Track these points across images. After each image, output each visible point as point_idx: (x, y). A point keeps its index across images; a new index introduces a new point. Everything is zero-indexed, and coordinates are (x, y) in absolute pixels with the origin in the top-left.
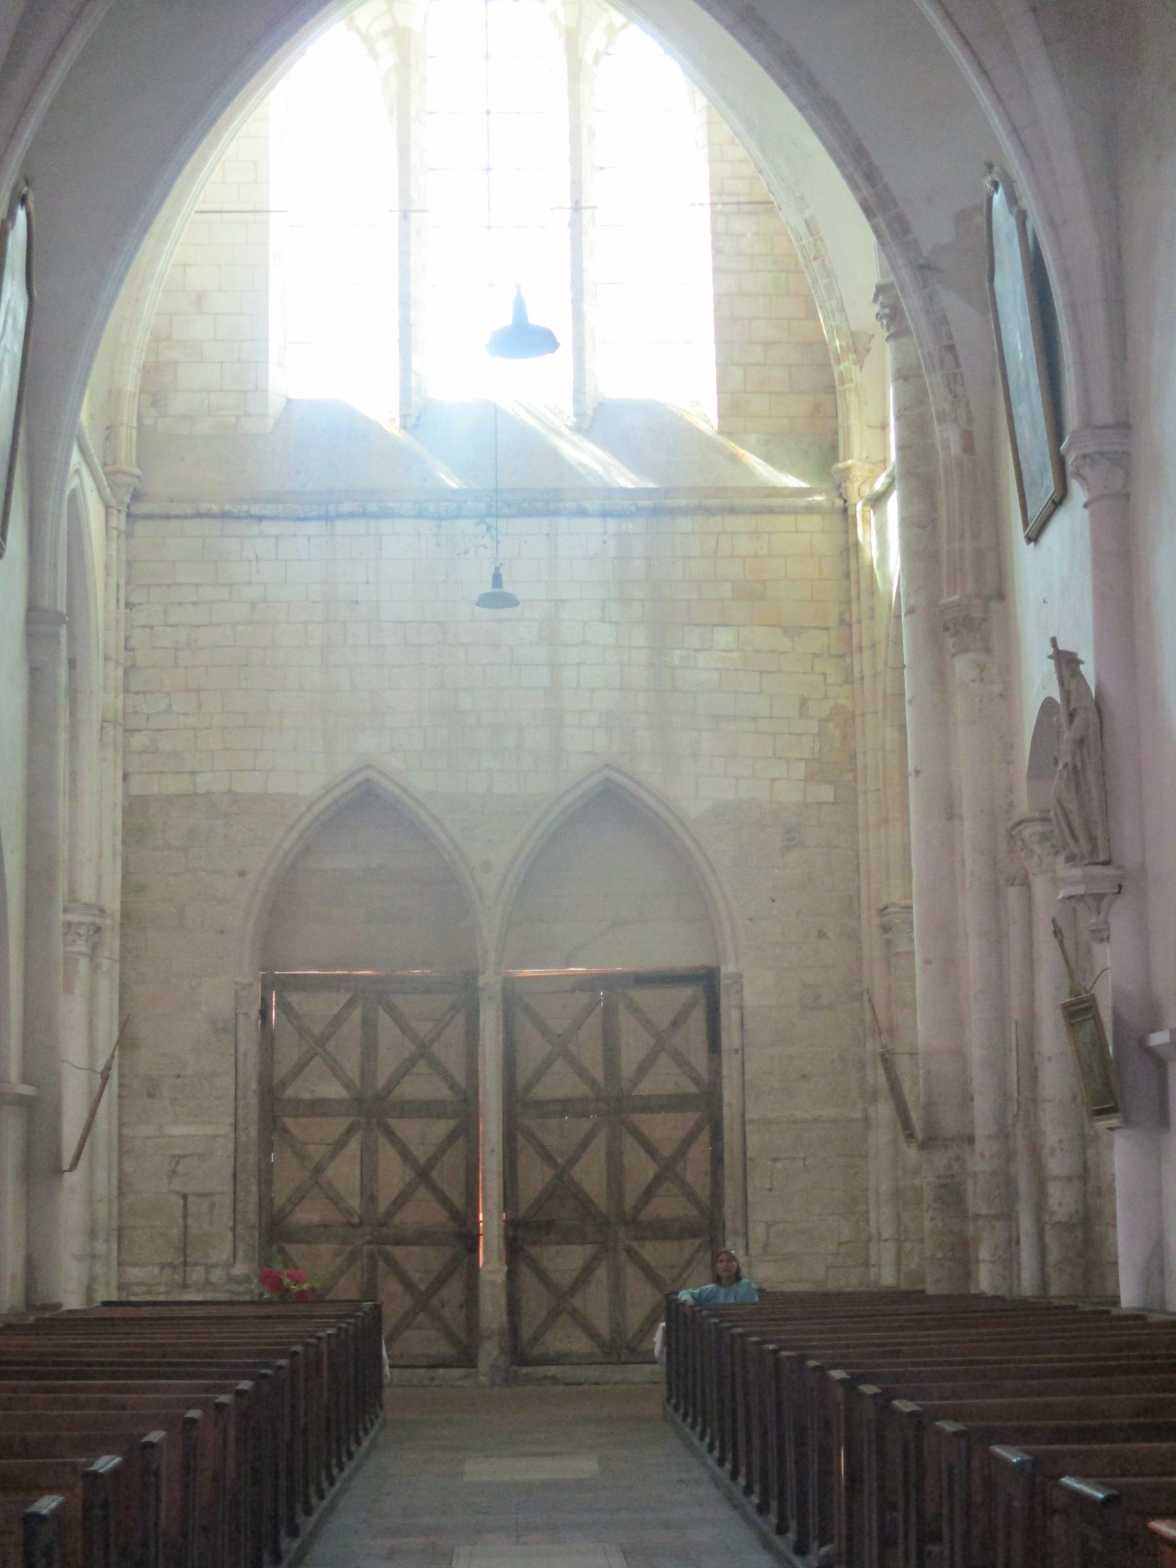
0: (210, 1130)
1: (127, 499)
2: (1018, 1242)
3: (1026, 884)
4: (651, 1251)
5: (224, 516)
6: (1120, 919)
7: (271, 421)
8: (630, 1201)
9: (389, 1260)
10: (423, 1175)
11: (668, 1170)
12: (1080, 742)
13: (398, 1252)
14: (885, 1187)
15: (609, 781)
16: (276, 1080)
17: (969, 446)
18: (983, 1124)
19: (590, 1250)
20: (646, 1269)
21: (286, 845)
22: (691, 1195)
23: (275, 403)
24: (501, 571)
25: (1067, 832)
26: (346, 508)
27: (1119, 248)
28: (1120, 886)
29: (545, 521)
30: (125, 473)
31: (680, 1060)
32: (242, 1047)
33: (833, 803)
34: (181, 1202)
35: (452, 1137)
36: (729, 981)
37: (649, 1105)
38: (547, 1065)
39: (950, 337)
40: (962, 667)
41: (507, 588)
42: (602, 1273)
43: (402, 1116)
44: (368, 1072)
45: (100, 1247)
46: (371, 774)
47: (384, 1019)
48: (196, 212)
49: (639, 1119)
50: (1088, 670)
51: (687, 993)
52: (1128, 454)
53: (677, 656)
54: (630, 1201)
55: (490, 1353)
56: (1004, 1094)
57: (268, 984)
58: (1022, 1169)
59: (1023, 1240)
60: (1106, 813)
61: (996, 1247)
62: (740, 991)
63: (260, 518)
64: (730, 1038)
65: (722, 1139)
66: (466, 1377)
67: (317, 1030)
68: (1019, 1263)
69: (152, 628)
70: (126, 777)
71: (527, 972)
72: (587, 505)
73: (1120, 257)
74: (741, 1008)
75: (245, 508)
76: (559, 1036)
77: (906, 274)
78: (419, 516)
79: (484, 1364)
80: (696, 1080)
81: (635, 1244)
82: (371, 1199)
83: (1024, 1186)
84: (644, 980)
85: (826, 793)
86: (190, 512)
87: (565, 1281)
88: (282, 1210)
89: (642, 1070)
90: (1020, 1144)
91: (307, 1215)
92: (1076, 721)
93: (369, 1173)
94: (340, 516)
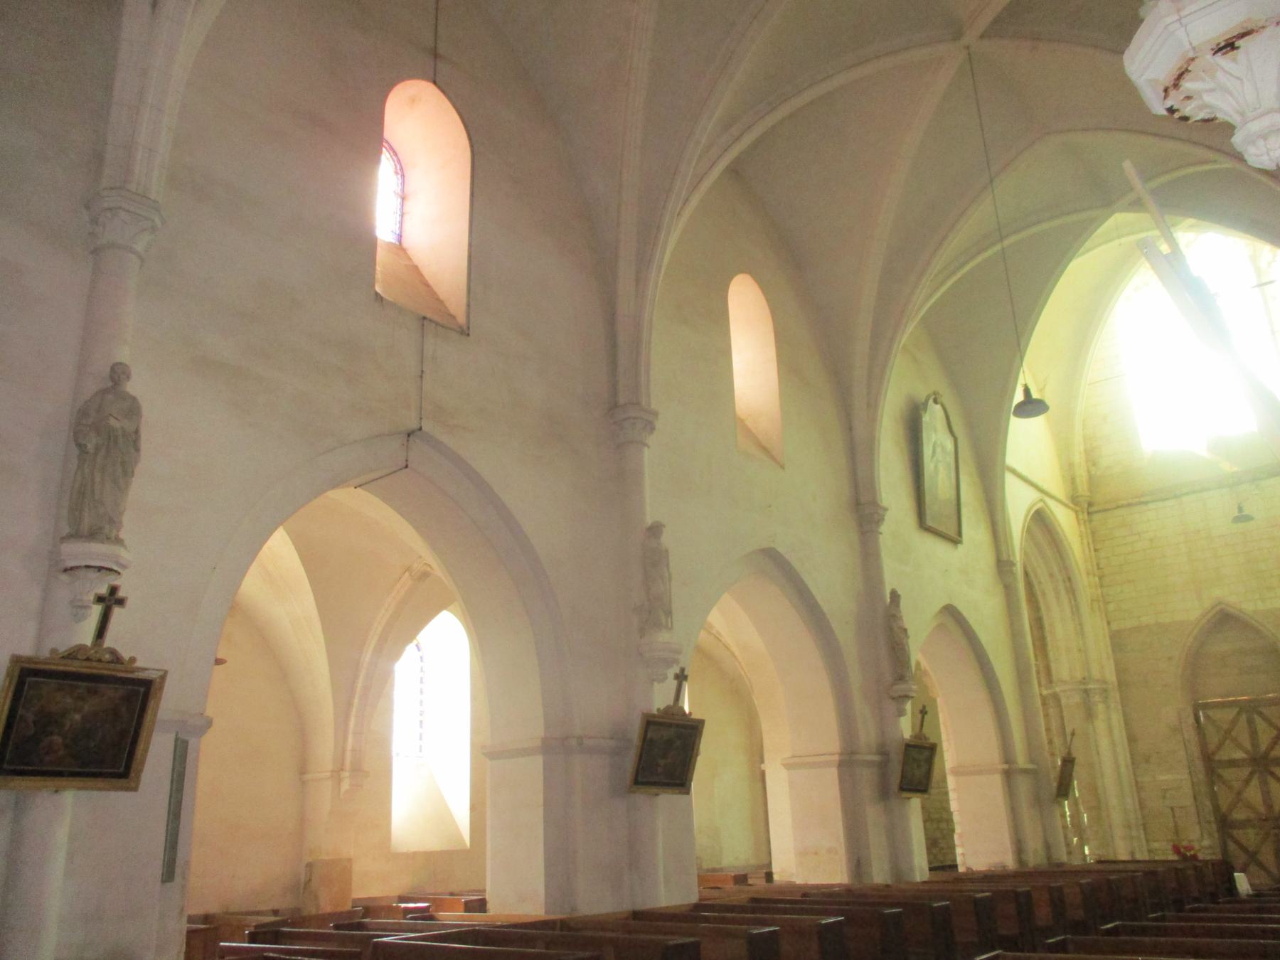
1: (1086, 506)
5: (1129, 505)
30: (1082, 496)
32: (1186, 736)
41: (1246, 512)
44: (1255, 744)
45: (1134, 833)
46: (1223, 606)
47: (1258, 720)
48: (1089, 384)
57: (1197, 708)
70: (1109, 623)
75: (1137, 500)
91: (1239, 815)
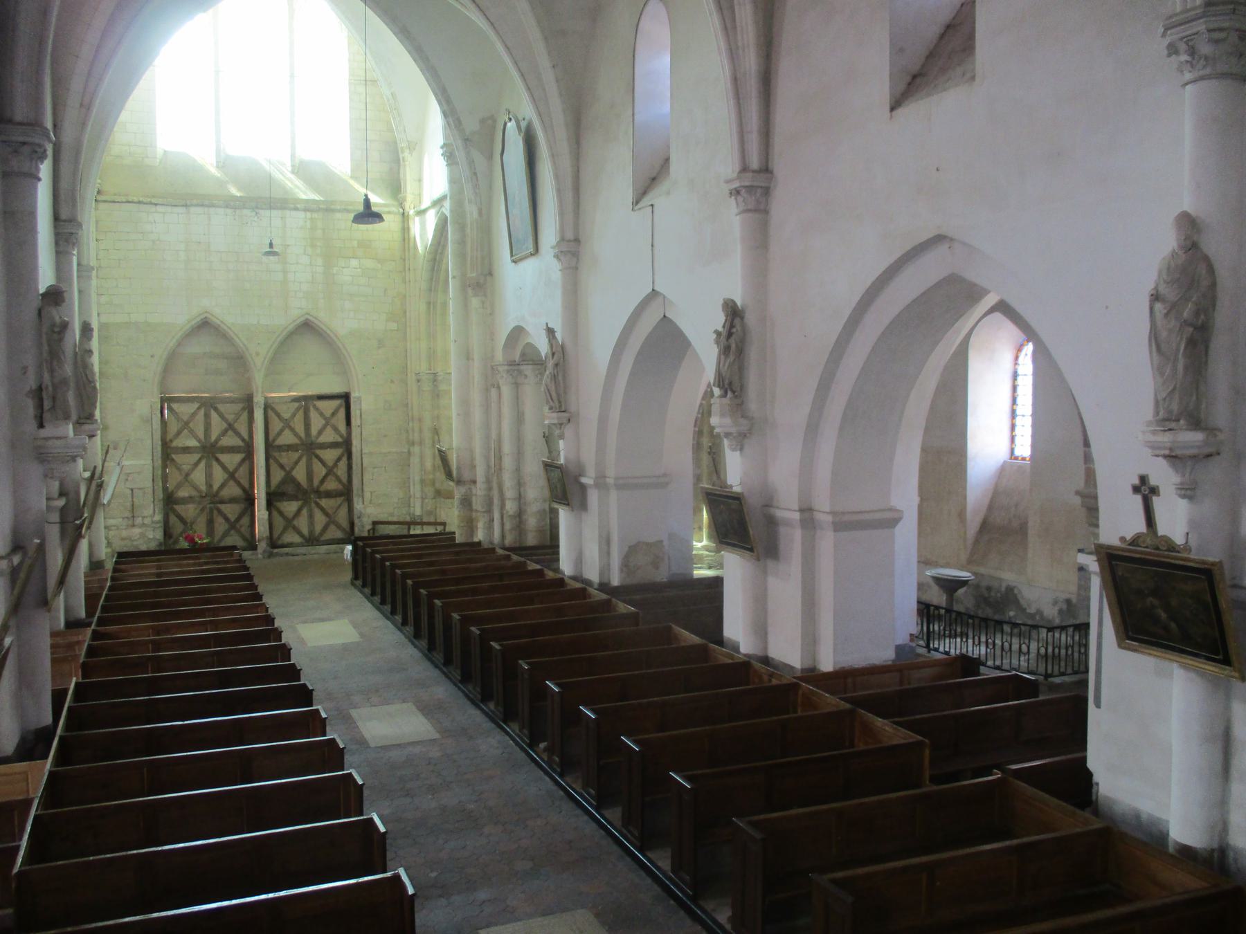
0: (142, 462)
2: (493, 520)
3: (499, 388)
4: (324, 502)
6: (568, 431)
7: (158, 161)
8: (316, 483)
9: (220, 512)
10: (232, 476)
11: (330, 472)
12: (557, 365)
13: (222, 507)
14: (417, 478)
15: (307, 319)
16: (168, 440)
17: (480, 213)
18: (480, 478)
19: (300, 503)
20: (322, 509)
21: (171, 344)
22: (340, 481)
23: (160, 153)
24: (273, 242)
25: (549, 398)
26: (195, 202)
27: (578, 168)
28: (569, 420)
29: (280, 212)
31: (336, 429)
33: (397, 330)
34: (131, 492)
35: (243, 461)
36: (355, 400)
37: (324, 446)
38: (282, 431)
39: (475, 169)
40: (475, 302)
42: (305, 512)
43: (222, 453)
49: (318, 452)
50: (559, 336)
51: (336, 403)
52: (579, 252)
53: (335, 270)
54: (316, 483)
55: (262, 546)
56: (489, 467)
57: (163, 400)
58: (495, 493)
59: (495, 520)
60: (565, 393)
61: (485, 522)
62: (360, 403)
63: (156, 204)
64: (355, 421)
65: (352, 459)
66: (252, 554)
67: (185, 418)
68: (493, 529)
69: (108, 250)
71: (273, 395)
72: (299, 206)
73: (578, 171)
74: (361, 410)
75: (149, 200)
76: (286, 420)
77: (459, 142)
78: (227, 207)
79: (260, 550)
80: (341, 436)
81: (318, 500)
82: (209, 485)
83: (496, 501)
84: (321, 397)
85: (394, 326)
86: (124, 200)
87: (290, 515)
88: (173, 491)
89: (320, 433)
90: (495, 485)
91: (183, 493)
92: (556, 356)
93: (209, 476)
94: (192, 205)
